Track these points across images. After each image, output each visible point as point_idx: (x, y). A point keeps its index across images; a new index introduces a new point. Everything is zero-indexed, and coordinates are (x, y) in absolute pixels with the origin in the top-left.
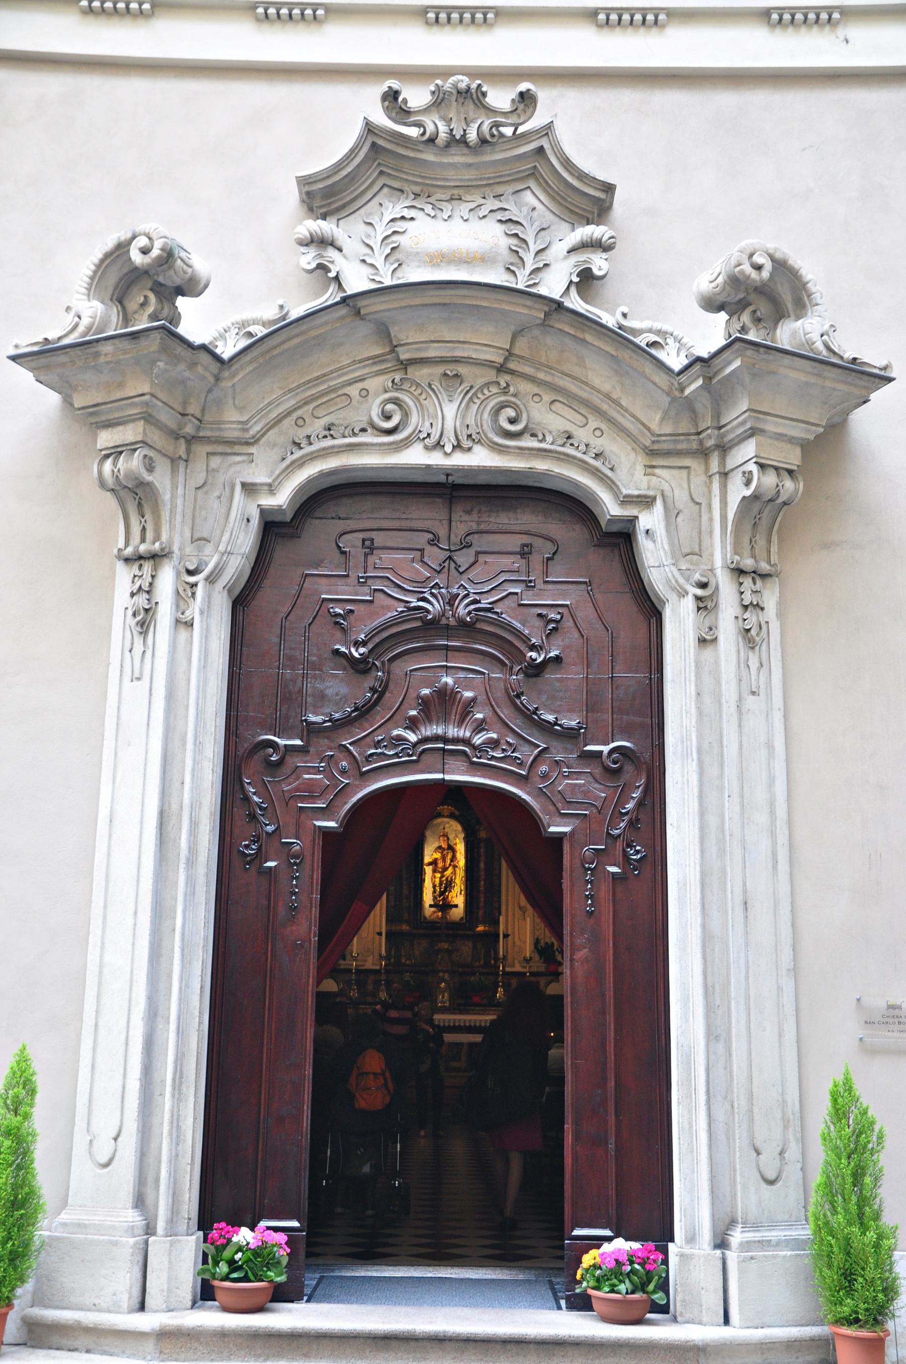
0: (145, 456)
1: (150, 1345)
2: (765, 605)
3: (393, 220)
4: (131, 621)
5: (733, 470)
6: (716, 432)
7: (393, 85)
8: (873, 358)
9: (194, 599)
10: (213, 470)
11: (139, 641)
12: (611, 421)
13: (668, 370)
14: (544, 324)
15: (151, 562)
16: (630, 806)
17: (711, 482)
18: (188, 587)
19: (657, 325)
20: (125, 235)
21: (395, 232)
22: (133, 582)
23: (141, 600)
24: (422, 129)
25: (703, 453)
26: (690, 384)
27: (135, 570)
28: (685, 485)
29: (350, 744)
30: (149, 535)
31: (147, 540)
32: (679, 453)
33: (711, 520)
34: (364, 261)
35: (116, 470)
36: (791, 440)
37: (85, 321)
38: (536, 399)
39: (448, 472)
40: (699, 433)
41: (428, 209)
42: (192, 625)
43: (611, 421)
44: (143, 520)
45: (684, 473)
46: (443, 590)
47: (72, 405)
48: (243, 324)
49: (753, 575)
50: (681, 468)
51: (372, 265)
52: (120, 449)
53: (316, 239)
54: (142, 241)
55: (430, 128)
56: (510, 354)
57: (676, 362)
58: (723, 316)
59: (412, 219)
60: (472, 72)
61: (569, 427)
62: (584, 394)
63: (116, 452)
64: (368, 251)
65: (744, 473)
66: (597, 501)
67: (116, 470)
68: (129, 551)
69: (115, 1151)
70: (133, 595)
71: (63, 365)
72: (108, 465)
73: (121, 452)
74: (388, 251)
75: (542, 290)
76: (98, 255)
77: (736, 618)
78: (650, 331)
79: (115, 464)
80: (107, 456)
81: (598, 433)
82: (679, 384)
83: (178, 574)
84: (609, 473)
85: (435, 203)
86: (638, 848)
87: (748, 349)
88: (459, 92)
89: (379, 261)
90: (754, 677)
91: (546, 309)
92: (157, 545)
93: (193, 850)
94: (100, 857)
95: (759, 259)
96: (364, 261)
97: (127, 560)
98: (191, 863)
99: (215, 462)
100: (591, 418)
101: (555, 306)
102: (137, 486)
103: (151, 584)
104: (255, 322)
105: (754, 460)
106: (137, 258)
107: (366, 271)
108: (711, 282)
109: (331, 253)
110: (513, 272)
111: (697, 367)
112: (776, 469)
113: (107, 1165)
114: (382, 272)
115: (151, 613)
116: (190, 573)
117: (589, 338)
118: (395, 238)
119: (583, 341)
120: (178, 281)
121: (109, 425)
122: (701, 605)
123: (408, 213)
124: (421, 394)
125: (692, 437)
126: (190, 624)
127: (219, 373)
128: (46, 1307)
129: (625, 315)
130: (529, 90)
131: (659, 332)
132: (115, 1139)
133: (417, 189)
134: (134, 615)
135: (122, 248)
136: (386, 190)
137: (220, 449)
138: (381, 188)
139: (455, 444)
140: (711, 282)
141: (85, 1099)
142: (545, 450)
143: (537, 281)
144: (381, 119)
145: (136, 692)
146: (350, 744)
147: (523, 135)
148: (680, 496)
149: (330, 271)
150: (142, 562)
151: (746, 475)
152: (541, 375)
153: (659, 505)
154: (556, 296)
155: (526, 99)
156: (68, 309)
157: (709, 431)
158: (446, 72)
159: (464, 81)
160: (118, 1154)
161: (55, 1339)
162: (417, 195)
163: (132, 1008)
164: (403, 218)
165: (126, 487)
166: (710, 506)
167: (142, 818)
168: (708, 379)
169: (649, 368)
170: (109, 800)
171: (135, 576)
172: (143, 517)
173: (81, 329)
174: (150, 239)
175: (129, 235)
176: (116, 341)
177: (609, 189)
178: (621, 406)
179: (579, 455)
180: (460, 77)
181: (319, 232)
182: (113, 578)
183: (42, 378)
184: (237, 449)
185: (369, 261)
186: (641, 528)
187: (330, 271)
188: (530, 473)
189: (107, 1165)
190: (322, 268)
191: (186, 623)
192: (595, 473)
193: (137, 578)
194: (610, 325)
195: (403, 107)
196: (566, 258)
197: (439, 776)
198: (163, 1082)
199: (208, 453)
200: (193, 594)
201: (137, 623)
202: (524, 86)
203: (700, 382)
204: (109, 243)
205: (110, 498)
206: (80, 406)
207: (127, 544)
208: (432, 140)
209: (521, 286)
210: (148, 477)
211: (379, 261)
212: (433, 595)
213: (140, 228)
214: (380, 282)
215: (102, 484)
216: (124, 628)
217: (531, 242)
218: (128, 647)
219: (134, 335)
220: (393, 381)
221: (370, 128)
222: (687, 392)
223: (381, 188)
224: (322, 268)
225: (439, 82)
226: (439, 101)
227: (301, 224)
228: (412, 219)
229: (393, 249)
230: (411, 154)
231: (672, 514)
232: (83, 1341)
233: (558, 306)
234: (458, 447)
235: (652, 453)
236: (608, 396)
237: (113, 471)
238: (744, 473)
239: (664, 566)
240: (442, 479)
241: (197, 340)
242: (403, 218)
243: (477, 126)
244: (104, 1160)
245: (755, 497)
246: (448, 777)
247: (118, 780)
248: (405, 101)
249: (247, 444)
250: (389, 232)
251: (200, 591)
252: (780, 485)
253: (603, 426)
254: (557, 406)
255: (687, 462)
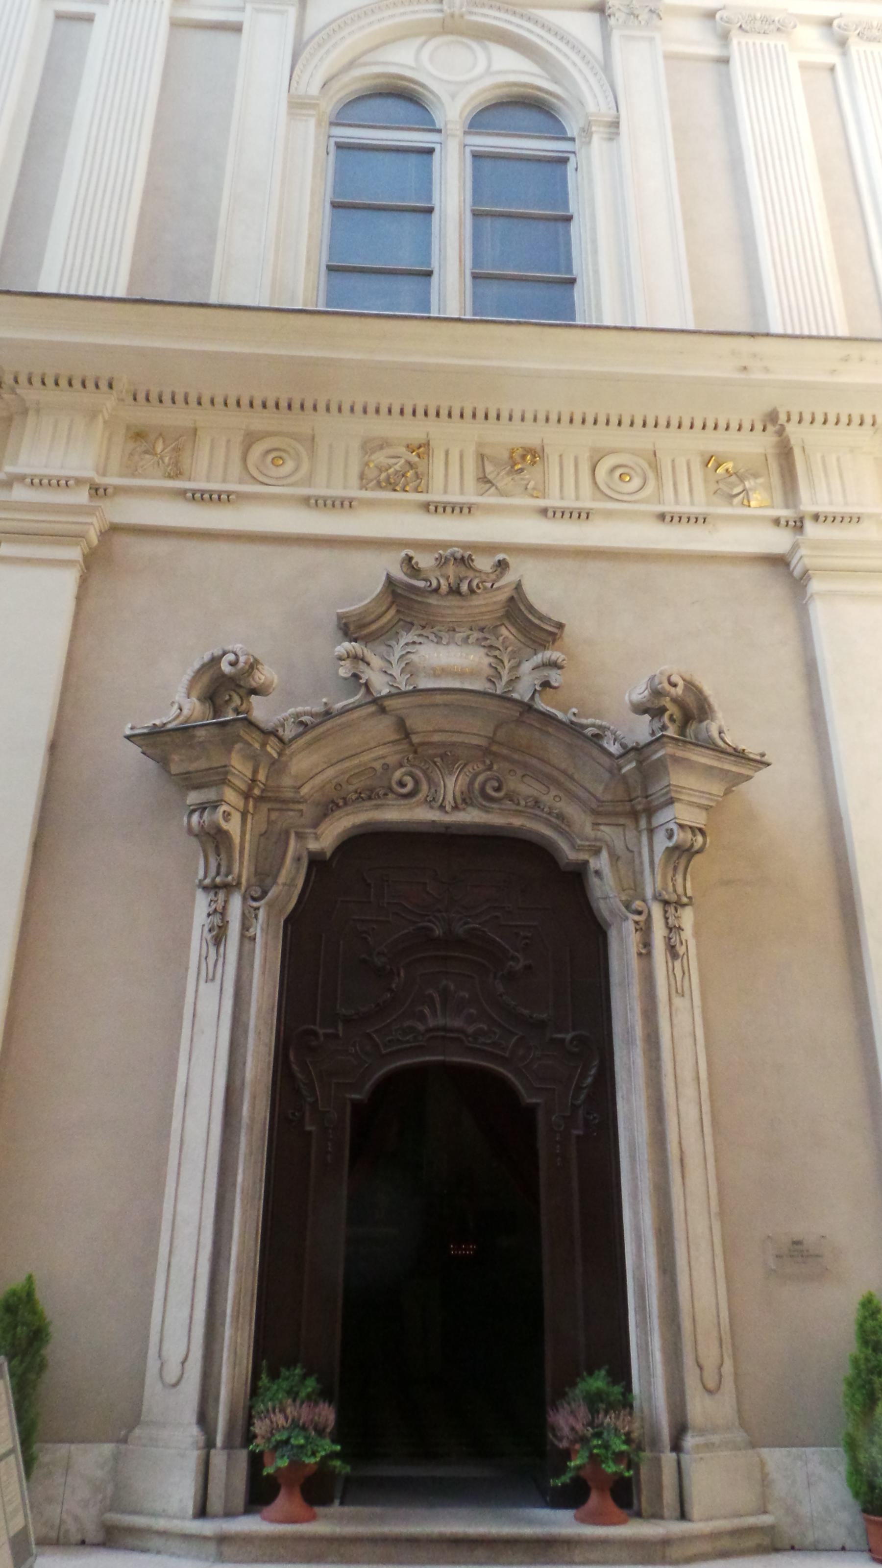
0: (224, 812)
1: (212, 1548)
2: (683, 926)
3: (407, 644)
4: (209, 936)
5: (657, 827)
6: (644, 800)
7: (409, 553)
8: (752, 749)
9: (257, 919)
10: (272, 821)
11: (212, 950)
12: (568, 792)
13: (610, 755)
14: (519, 722)
15: (225, 890)
16: (589, 1080)
17: (640, 835)
18: (252, 910)
19: (598, 722)
20: (217, 652)
21: (408, 653)
22: (210, 905)
23: (217, 920)
24: (429, 584)
25: (635, 815)
26: (626, 765)
27: (211, 895)
28: (623, 838)
29: (376, 1031)
30: (223, 870)
31: (222, 873)
32: (617, 814)
33: (641, 863)
34: (385, 672)
35: (202, 821)
36: (699, 806)
37: (186, 712)
38: (512, 773)
39: (448, 826)
40: (631, 801)
41: (432, 637)
42: (255, 939)
43: (568, 792)
44: (218, 858)
45: (621, 829)
46: (444, 914)
47: (169, 772)
48: (298, 715)
49: (674, 904)
50: (617, 825)
51: (391, 675)
52: (204, 806)
53: (351, 655)
54: (231, 657)
55: (435, 584)
56: (492, 740)
57: (614, 749)
58: (647, 717)
59: (420, 643)
60: (466, 546)
61: (535, 793)
62: (547, 769)
63: (202, 808)
64: (387, 664)
65: (667, 830)
66: (558, 849)
67: (202, 821)
68: (207, 881)
69: (183, 1374)
70: (209, 915)
71: (166, 743)
72: (195, 818)
73: (205, 808)
74: (403, 665)
75: (515, 696)
76: (197, 665)
77: (665, 937)
78: (593, 725)
79: (201, 817)
80: (194, 811)
81: (558, 799)
82: (617, 765)
83: (244, 899)
84: (567, 829)
85: (437, 633)
86: (595, 1115)
87: (670, 743)
88: (455, 559)
89: (396, 671)
90: (679, 983)
91: (521, 710)
92: (230, 878)
93: (252, 1119)
94: (176, 1124)
95: (675, 679)
96: (385, 672)
97: (205, 888)
98: (251, 1129)
99: (274, 816)
100: (552, 788)
101: (527, 708)
102: (216, 834)
103: (224, 908)
104: (306, 714)
105: (674, 821)
106: (225, 668)
107: (386, 679)
108: (640, 694)
109: (362, 666)
110: (494, 683)
111: (632, 754)
112: (691, 827)
113: (175, 1385)
114: (398, 680)
115: (223, 929)
116: (255, 899)
117: (550, 730)
118: (409, 656)
119: (547, 732)
120: (254, 684)
121: (198, 787)
122: (638, 927)
123: (416, 639)
124: (428, 768)
125: (627, 803)
126: (253, 939)
127: (282, 750)
128: (124, 1512)
129: (574, 714)
130: (504, 559)
131: (600, 727)
132: (183, 1363)
133: (423, 623)
134: (210, 931)
135: (215, 661)
136: (401, 623)
137: (278, 806)
138: (398, 622)
139: (454, 805)
140: (640, 694)
141: (158, 1328)
142: (520, 811)
143: (511, 689)
144: (399, 574)
145: (209, 992)
146: (376, 1031)
147: (499, 588)
148: (619, 846)
149: (361, 678)
150: (217, 890)
151: (669, 831)
152: (516, 756)
153: (604, 854)
154: (526, 699)
155: (502, 565)
156: (173, 703)
157: (640, 799)
158: (445, 545)
159: (459, 552)
160: (185, 1376)
161: (130, 1541)
162: (424, 627)
163: (200, 1250)
164: (414, 643)
165: (208, 833)
166: (640, 853)
167: (212, 1092)
168: (640, 762)
169: (595, 752)
170: (185, 1078)
171: (211, 901)
172: (219, 855)
173: (181, 718)
174: (236, 655)
175: (220, 652)
176: (208, 728)
177: (560, 626)
178: (574, 780)
179: (545, 815)
180: (456, 549)
181: (353, 651)
182: (193, 900)
183: (148, 752)
184: (291, 806)
185: (389, 672)
186: (592, 869)
187: (361, 678)
188: (510, 827)
189: (175, 1385)
190: (356, 676)
191: (250, 937)
192: (556, 828)
193: (212, 903)
194: (564, 720)
195: (415, 567)
196: (530, 673)
197: (441, 1058)
198: (224, 1312)
199: (269, 810)
200: (256, 917)
201: (213, 937)
202: (501, 556)
203: (634, 764)
204: (207, 657)
205: (195, 843)
206: (177, 772)
207: (205, 877)
208: (436, 590)
209: (498, 692)
210: (225, 826)
211: (396, 671)
212: (435, 917)
213: (229, 647)
214: (397, 687)
215: (190, 830)
216: (201, 940)
217: (506, 662)
218: (204, 954)
219: (224, 724)
220: (408, 759)
221: (390, 582)
222: (624, 771)
223: (398, 622)
224: (356, 676)
225: (441, 552)
226: (442, 562)
227: (340, 645)
228: (420, 643)
229: (407, 664)
230: (420, 599)
231: (614, 858)
232: (157, 1542)
233: (528, 708)
234: (456, 808)
235: (595, 813)
236: (564, 772)
237: (199, 822)
238: (667, 830)
239: (609, 897)
240: (442, 830)
241: (268, 725)
242: (414, 643)
243: (468, 581)
244: (174, 1380)
245: (676, 848)
246: (448, 1059)
247: (193, 1059)
248: (417, 563)
249: (299, 802)
250: (404, 652)
251: (261, 914)
252: (694, 839)
253: (561, 794)
254: (526, 779)
255: (622, 821)
